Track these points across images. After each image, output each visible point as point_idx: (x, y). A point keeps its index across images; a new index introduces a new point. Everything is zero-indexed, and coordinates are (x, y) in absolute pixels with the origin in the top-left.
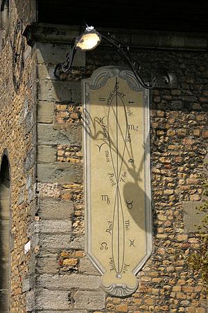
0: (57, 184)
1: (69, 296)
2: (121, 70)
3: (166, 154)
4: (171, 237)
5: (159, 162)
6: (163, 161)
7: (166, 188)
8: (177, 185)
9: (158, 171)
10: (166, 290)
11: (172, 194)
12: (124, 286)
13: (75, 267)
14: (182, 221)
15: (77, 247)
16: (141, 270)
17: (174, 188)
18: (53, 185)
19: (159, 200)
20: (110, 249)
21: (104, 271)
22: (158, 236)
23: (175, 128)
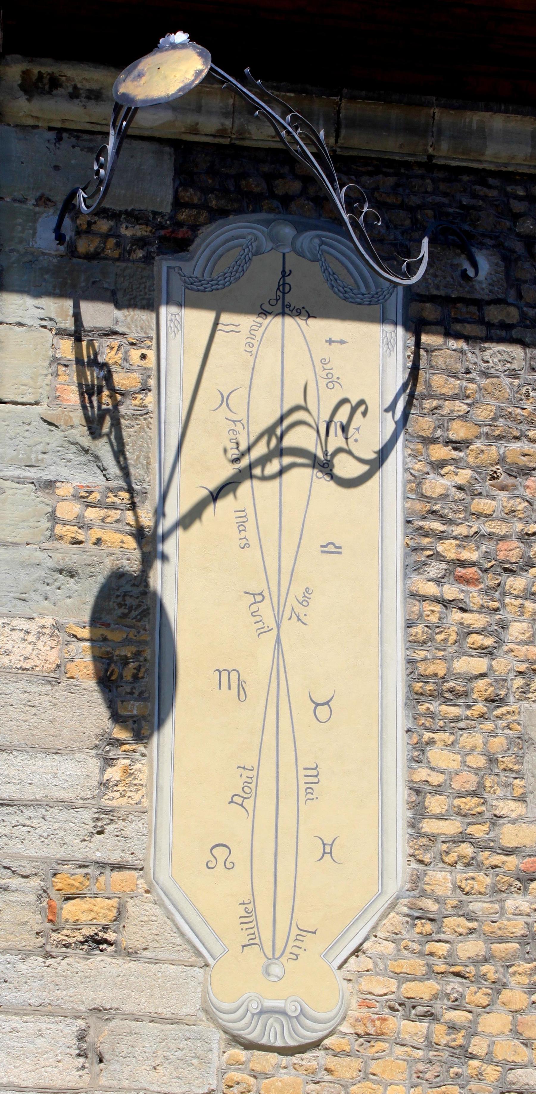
0: (48, 621)
1: (81, 1038)
2: (301, 228)
3: (461, 530)
4: (478, 831)
5: (437, 556)
6: (451, 555)
7: (461, 653)
8: (500, 642)
9: (431, 589)
10: (453, 1028)
11: (483, 676)
12: (292, 1010)
13: (105, 929)
14: (519, 775)
15: (115, 857)
16: (357, 952)
17: (487, 652)
18: (33, 626)
19: (432, 696)
20: (242, 867)
21: (217, 950)
22: (428, 826)
23: (500, 438)
